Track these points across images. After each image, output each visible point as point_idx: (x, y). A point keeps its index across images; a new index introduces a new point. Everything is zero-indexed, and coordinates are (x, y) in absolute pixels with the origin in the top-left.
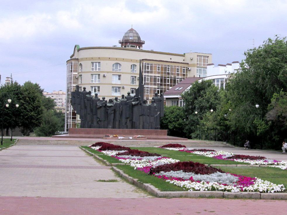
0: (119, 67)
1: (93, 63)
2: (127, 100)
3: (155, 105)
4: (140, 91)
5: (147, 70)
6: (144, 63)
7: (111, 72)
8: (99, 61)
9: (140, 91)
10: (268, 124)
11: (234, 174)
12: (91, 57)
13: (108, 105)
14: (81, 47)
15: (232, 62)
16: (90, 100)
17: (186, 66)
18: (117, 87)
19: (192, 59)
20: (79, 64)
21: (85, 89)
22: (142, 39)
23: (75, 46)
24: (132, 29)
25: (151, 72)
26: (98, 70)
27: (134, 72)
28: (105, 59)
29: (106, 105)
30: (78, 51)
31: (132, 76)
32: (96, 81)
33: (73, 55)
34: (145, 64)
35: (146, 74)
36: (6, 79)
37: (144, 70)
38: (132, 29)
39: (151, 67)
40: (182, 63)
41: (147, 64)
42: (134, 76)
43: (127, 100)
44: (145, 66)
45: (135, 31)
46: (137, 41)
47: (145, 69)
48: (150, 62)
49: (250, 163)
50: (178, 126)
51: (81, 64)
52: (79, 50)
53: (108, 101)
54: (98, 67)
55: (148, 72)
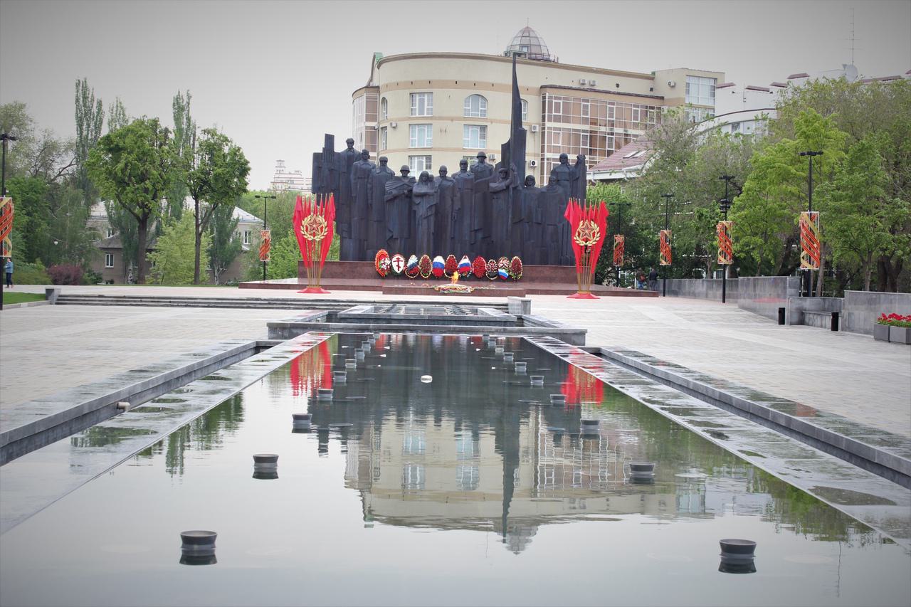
0: (482, 107)
2: (476, 179)
6: (547, 95)
7: (458, 119)
10: (47, 290)
13: (416, 190)
14: (385, 55)
16: (367, 174)
19: (672, 84)
20: (381, 98)
23: (374, 57)
24: (528, 27)
25: (567, 120)
28: (444, 84)
30: (378, 68)
32: (423, 139)
34: (550, 98)
36: (277, 164)
40: (646, 96)
41: (556, 98)
44: (550, 103)
47: (550, 111)
48: (563, 93)
50: (527, 538)
51: (384, 99)
54: (426, 107)
55: (557, 119)
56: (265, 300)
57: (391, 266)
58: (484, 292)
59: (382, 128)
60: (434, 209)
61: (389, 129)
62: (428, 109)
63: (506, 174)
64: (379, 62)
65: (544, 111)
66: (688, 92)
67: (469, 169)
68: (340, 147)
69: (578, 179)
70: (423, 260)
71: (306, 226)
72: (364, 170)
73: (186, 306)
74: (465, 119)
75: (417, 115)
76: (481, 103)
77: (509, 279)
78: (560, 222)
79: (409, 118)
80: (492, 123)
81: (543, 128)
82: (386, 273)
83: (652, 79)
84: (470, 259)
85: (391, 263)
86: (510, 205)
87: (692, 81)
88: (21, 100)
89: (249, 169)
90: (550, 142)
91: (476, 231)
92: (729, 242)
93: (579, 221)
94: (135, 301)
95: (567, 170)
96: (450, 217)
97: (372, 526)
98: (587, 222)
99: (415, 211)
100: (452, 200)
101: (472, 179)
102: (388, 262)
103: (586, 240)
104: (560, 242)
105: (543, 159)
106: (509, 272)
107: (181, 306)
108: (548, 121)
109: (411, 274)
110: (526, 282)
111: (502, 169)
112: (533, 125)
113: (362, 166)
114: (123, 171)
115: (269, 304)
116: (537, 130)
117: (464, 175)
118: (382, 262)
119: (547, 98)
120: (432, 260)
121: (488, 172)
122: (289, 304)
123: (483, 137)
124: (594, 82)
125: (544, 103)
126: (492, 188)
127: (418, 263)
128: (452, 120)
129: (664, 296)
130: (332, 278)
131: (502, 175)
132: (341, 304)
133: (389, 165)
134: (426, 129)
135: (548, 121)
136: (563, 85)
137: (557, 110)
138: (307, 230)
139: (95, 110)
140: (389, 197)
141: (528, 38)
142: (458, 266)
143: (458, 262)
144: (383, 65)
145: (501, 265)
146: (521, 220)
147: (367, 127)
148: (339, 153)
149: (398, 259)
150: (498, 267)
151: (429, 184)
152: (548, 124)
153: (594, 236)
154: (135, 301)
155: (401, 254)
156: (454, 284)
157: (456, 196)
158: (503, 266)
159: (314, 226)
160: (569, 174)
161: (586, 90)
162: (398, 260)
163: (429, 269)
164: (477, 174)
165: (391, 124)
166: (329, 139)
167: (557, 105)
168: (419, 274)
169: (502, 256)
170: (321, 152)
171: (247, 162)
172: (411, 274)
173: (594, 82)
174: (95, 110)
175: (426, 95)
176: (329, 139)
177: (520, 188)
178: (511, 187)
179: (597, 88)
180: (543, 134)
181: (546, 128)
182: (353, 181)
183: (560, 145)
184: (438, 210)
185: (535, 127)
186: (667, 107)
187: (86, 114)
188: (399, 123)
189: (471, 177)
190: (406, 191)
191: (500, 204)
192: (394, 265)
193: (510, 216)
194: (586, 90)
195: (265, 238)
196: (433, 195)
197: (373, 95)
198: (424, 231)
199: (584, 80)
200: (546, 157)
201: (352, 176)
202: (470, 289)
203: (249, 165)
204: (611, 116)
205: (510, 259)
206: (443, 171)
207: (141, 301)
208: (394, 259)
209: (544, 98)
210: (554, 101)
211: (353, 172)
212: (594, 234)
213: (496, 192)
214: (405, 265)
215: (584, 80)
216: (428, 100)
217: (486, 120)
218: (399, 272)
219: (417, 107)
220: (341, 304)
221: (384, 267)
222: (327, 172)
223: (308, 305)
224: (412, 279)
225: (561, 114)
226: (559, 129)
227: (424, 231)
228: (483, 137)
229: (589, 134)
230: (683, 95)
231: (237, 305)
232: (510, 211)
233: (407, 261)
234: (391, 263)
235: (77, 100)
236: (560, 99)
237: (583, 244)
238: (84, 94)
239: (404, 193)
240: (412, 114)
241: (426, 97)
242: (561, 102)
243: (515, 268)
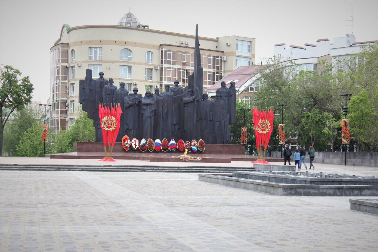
0: (129, 56)
2: (174, 95)
3: (222, 102)
4: (196, 79)
5: (167, 60)
6: (164, 49)
7: (117, 62)
8: (100, 46)
9: (196, 79)
14: (71, 26)
15: (317, 40)
17: (219, 54)
19: (229, 44)
21: (101, 74)
23: (64, 27)
24: (129, 13)
25: (174, 63)
26: (99, 59)
27: (149, 62)
28: (108, 43)
29: (140, 102)
30: (68, 33)
31: (147, 69)
33: (60, 40)
34: (166, 51)
37: (164, 60)
41: (168, 51)
42: (149, 69)
43: (174, 95)
44: (165, 54)
47: (165, 58)
48: (172, 49)
49: (81, 147)
52: (69, 31)
53: (143, 96)
54: (98, 55)
55: (169, 63)
56: (114, 166)
57: (131, 145)
58: (208, 160)
59: (71, 67)
60: (154, 112)
61: (76, 68)
62: (99, 56)
63: (192, 93)
65: (162, 58)
66: (237, 49)
68: (95, 76)
69: (232, 95)
70: (149, 141)
71: (105, 122)
72: (111, 90)
73: (69, 170)
74: (120, 62)
75: (93, 60)
76: (129, 53)
77: (198, 152)
78: (223, 119)
79: (89, 61)
80: (135, 64)
81: (162, 68)
82: (129, 149)
83: (217, 41)
84: (175, 141)
85: (131, 143)
86: (195, 110)
87: (239, 43)
89: (33, 89)
90: (165, 75)
91: (175, 124)
92: (348, 130)
93: (259, 119)
94: (37, 168)
95: (226, 91)
96: (161, 117)
98: (110, 117)
99: (143, 114)
100: (163, 107)
101: (172, 95)
102: (129, 142)
104: (223, 131)
105: (161, 85)
106: (197, 148)
107: (66, 170)
108: (164, 64)
109: (142, 150)
110: (207, 153)
111: (190, 90)
112: (156, 66)
113: (110, 88)
115: (118, 168)
116: (158, 69)
118: (126, 143)
119: (164, 51)
120: (154, 142)
121: (181, 92)
122: (129, 169)
123: (130, 72)
124: (188, 42)
125: (162, 54)
126: (184, 100)
127: (146, 143)
128: (113, 63)
129: (346, 165)
130: (97, 152)
131: (190, 93)
132: (160, 168)
134: (98, 67)
135: (164, 64)
136: (171, 44)
137: (169, 58)
138: (105, 125)
140: (128, 105)
141: (130, 19)
142: (169, 145)
143: (169, 142)
144: (71, 32)
145: (193, 144)
146: (201, 119)
147: (62, 66)
148: (95, 80)
149: (135, 141)
150: (191, 145)
151: (151, 98)
152: (164, 65)
153: (267, 128)
154: (37, 168)
155: (136, 138)
156: (184, 156)
157: (164, 105)
158: (195, 145)
159: (109, 122)
160: (227, 93)
161: (184, 47)
162: (135, 142)
163: (153, 147)
164: (175, 93)
165: (78, 64)
167: (169, 55)
168: (147, 149)
169: (194, 139)
170: (84, 79)
171: (32, 85)
172: (142, 150)
173: (188, 42)
175: (98, 48)
177: (200, 101)
178: (196, 100)
179: (189, 46)
180: (162, 71)
181: (163, 68)
182: (104, 96)
183: (171, 77)
184: (155, 113)
185: (157, 67)
186: (226, 57)
188: (82, 64)
189: (172, 94)
190: (137, 102)
191: (189, 110)
192: (133, 144)
193: (195, 116)
194: (184, 47)
195: (45, 129)
196: (153, 104)
197: (65, 48)
198: (148, 124)
199: (182, 42)
200: (163, 83)
201: (103, 94)
202: (199, 159)
203: (33, 87)
204: (184, 59)
205: (198, 141)
206: (157, 91)
207: (41, 168)
208: (133, 141)
209: (162, 51)
210: (167, 53)
211: (104, 91)
212: (114, 124)
213: (187, 103)
214: (139, 144)
215: (182, 42)
216: (99, 51)
217: (132, 63)
218: (136, 148)
219: (93, 55)
220: (160, 168)
221: (128, 145)
222: (88, 91)
223: (140, 169)
224: (165, 152)
225: (171, 60)
226: (170, 68)
227: (148, 124)
228: (130, 72)
229: (186, 71)
230: (235, 50)
231: (99, 170)
232: (195, 113)
233: (140, 142)
234: (131, 143)
236: (170, 51)
237: (107, 129)
239: (136, 103)
240: (90, 59)
241: (98, 50)
242: (171, 53)
243: (201, 146)
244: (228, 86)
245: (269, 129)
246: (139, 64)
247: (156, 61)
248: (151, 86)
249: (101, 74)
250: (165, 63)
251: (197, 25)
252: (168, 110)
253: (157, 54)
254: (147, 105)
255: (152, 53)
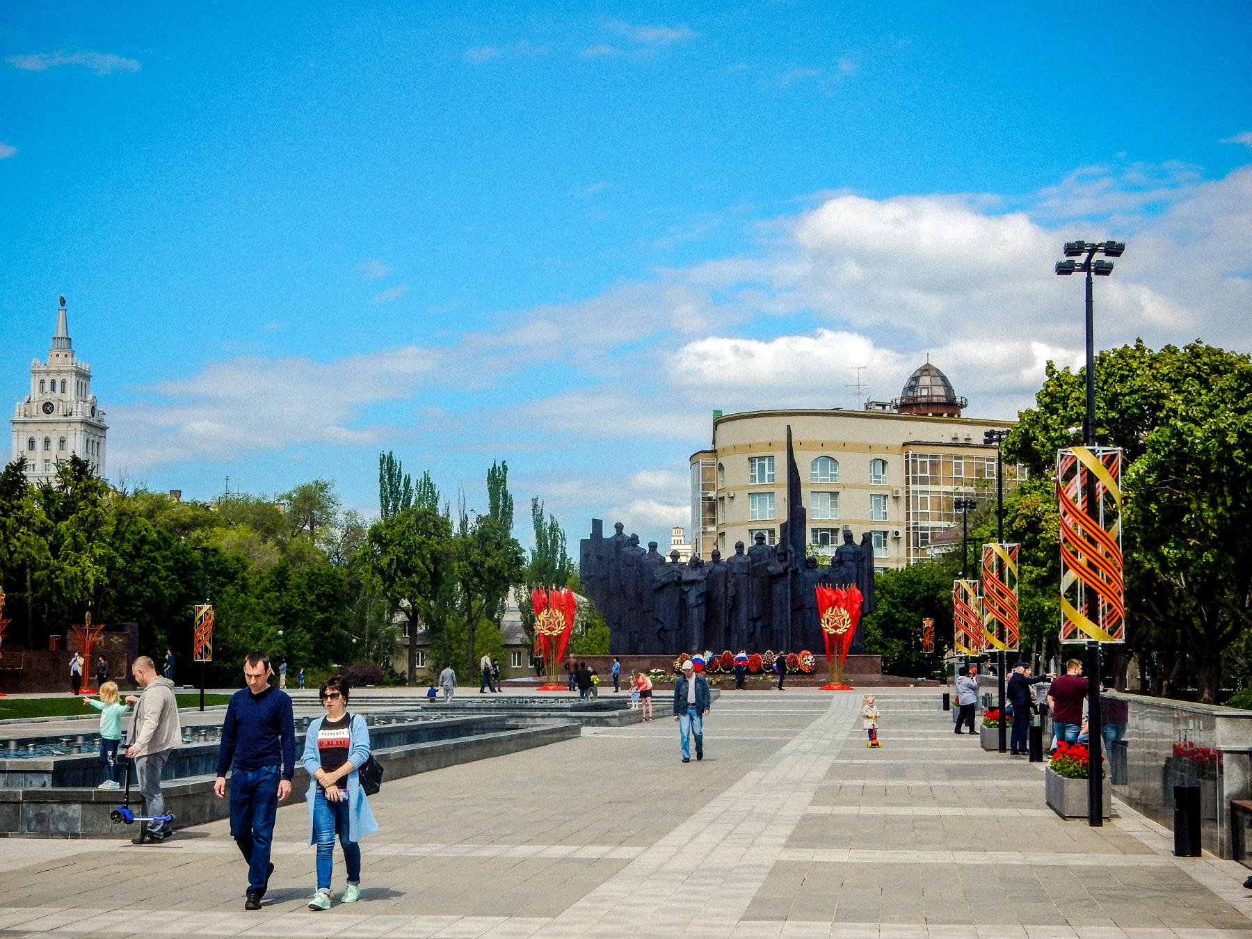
1: (751, 459)
2: (753, 562)
8: (770, 454)
11: (395, 900)
12: (747, 442)
18: (828, 530)
21: (619, 527)
22: (959, 393)
24: (928, 365)
35: (919, 487)
38: (928, 365)
39: (934, 465)
41: (921, 456)
45: (938, 370)
46: (943, 400)
48: (930, 450)
54: (767, 473)
55: (924, 481)
61: (890, 500)
64: (719, 421)
65: (907, 473)
67: (746, 552)
68: (608, 533)
81: (908, 492)
88: (325, 479)
97: (946, 707)
103: (836, 628)
114: (390, 565)
117: (741, 559)
123: (835, 505)
125: (907, 462)
133: (659, 550)
139: (402, 488)
166: (597, 524)
174: (402, 488)
176: (597, 524)
179: (973, 442)
180: (908, 498)
184: (708, 598)
185: (897, 492)
187: (392, 492)
209: (907, 457)
228: (835, 505)
235: (382, 477)
237: (833, 631)
238: (389, 470)
244: (858, 540)
245: (848, 624)
246: (854, 486)
247: (895, 477)
248: (885, 533)
249: (619, 527)
250: (915, 482)
251: (789, 427)
252: (737, 591)
253: (896, 463)
254: (692, 583)
255: (884, 463)
